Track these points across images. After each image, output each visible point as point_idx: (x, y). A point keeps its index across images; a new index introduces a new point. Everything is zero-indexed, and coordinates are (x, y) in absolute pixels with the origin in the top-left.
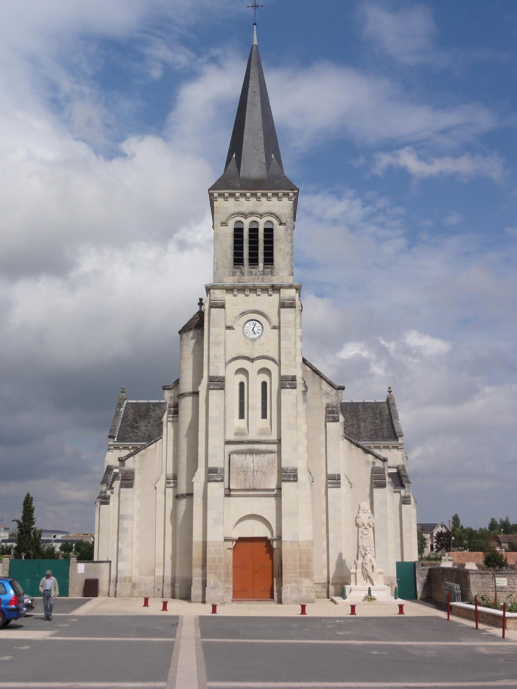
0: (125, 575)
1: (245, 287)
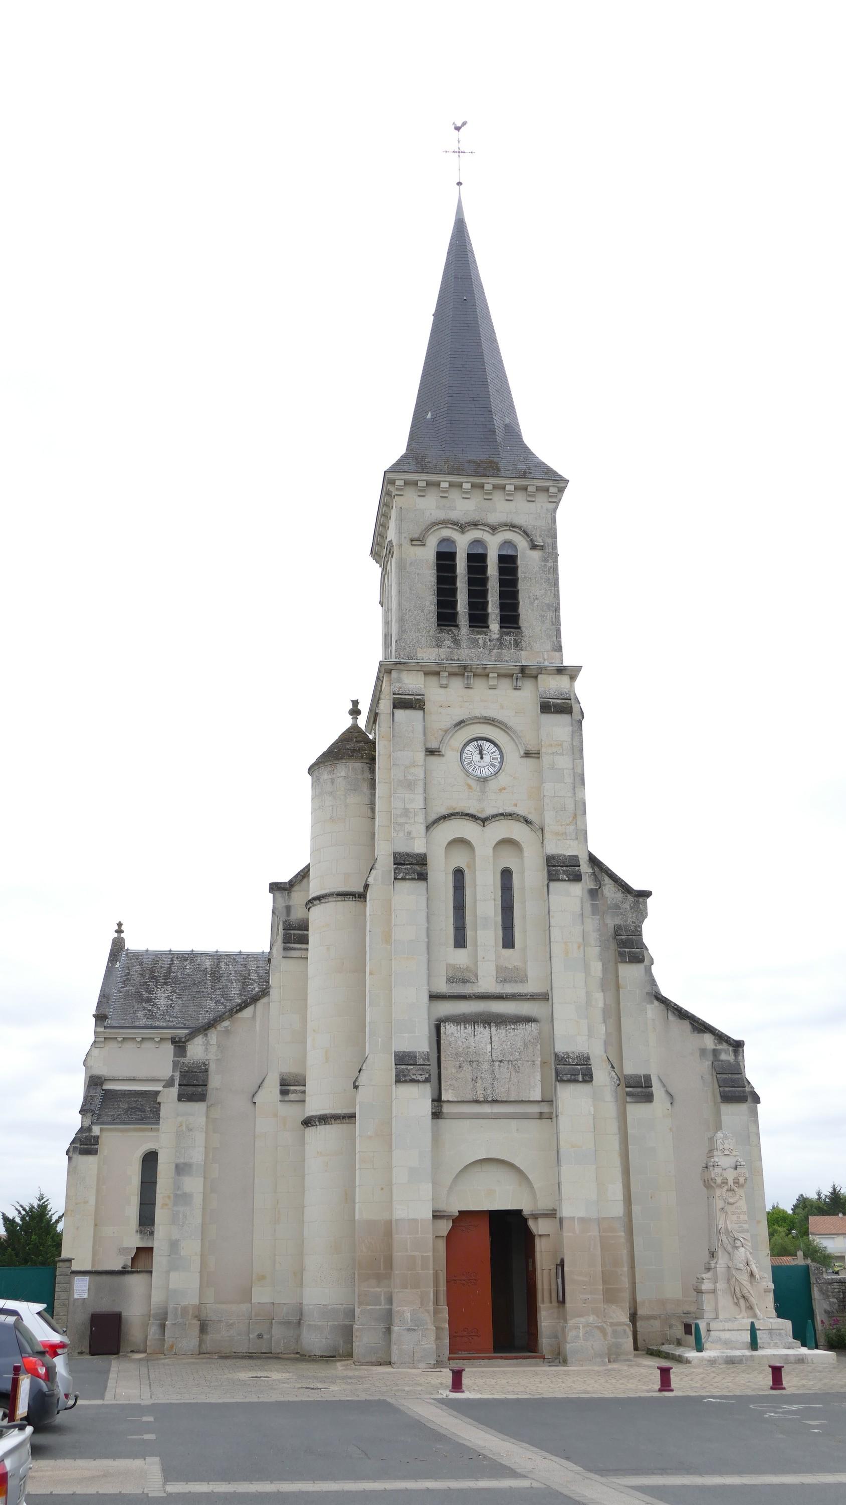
0: (185, 1303)
1: (465, 668)
